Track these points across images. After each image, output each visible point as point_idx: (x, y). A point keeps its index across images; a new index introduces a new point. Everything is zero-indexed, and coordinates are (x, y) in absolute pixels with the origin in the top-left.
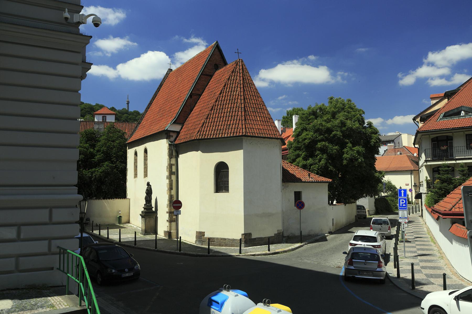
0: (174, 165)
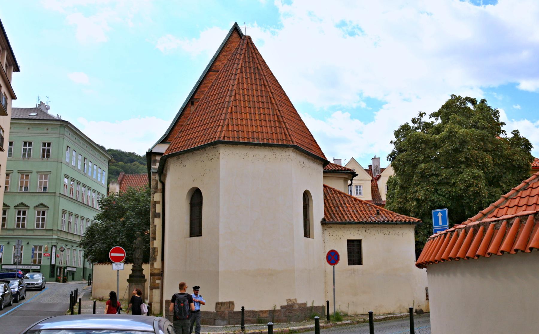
0: (158, 202)
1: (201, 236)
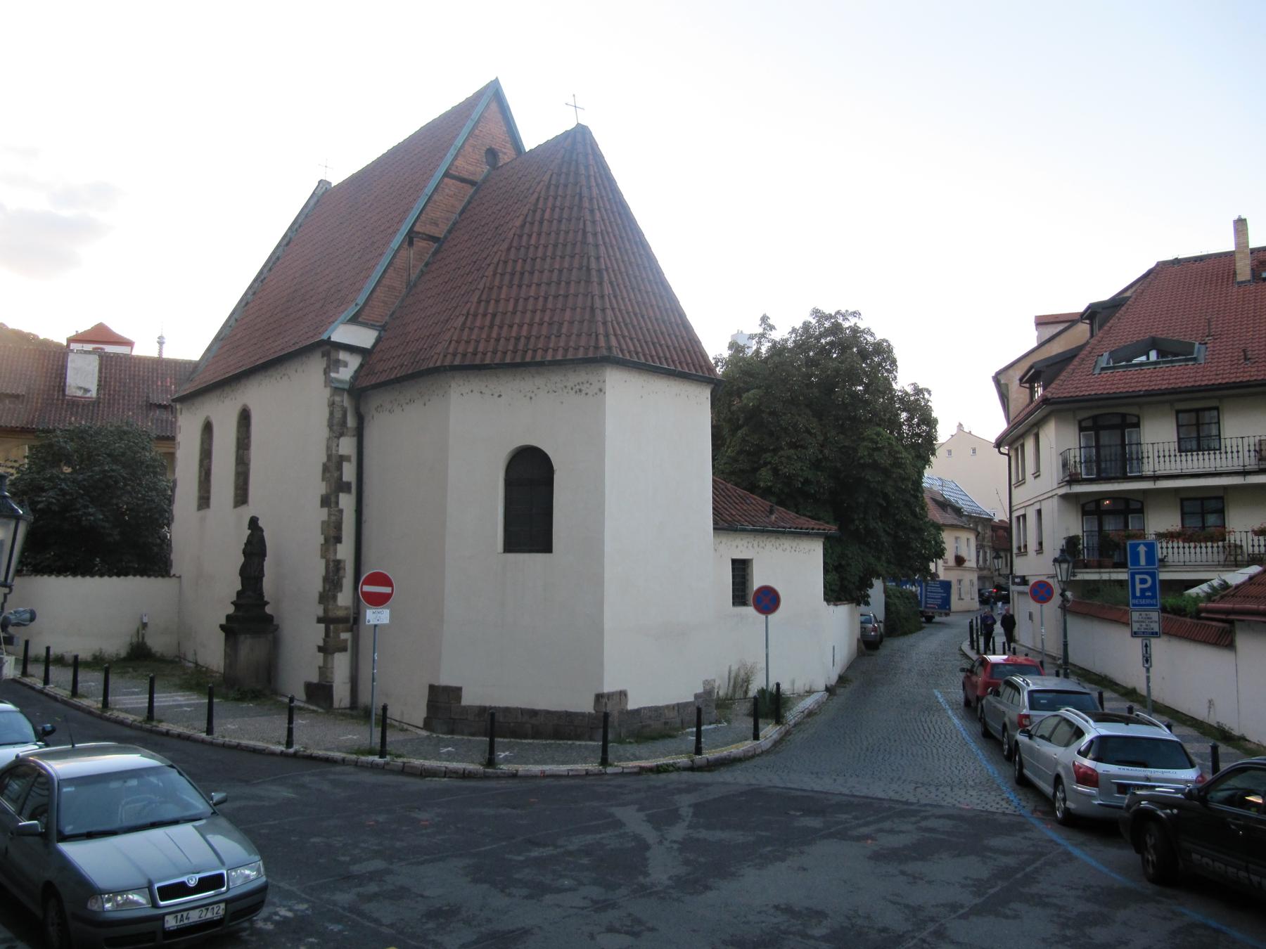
0: (348, 459)
1: (547, 547)
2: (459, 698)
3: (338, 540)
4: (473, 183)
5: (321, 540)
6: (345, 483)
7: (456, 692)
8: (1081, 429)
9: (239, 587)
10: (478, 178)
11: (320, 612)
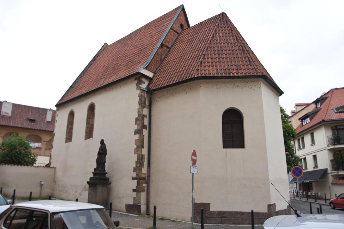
2: (209, 208)
3: (142, 147)
4: (178, 33)
5: (135, 147)
6: (145, 125)
7: (208, 205)
8: (332, 130)
9: (95, 167)
10: (179, 32)
11: (134, 175)
